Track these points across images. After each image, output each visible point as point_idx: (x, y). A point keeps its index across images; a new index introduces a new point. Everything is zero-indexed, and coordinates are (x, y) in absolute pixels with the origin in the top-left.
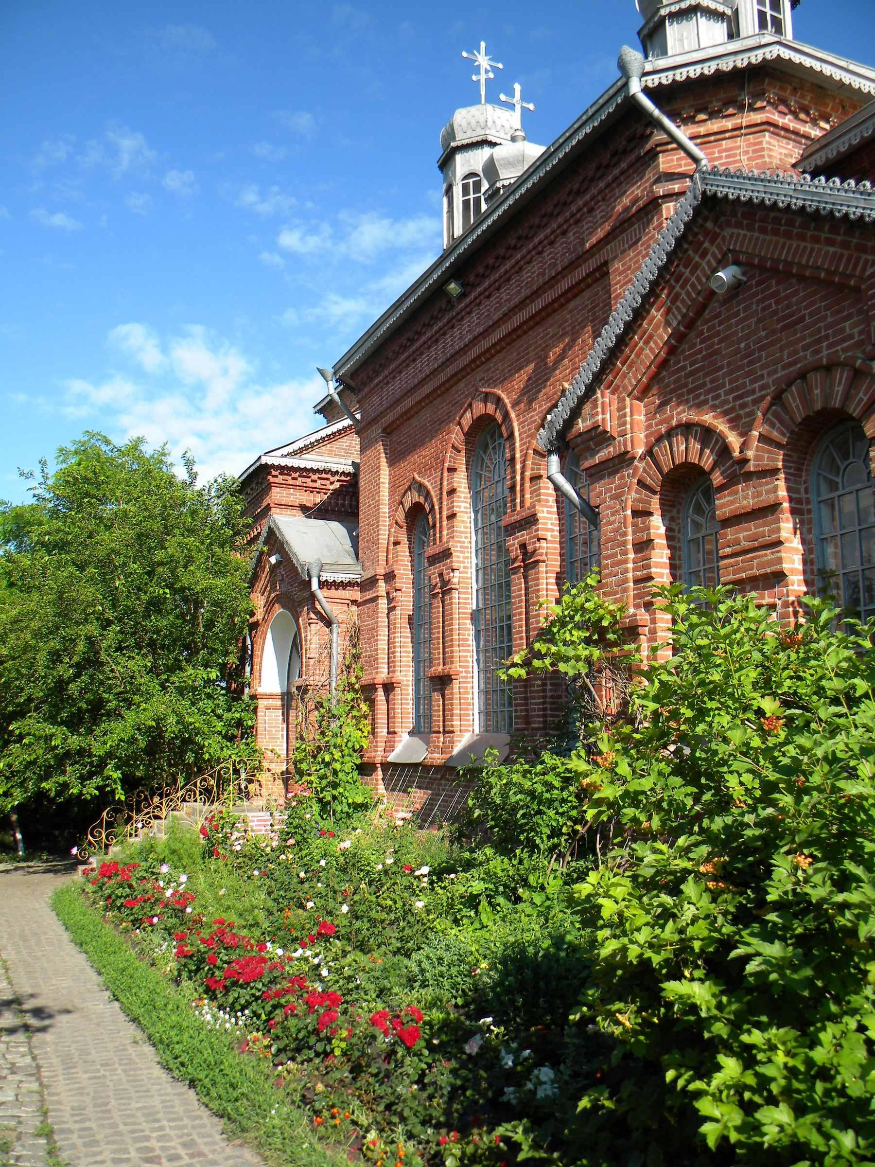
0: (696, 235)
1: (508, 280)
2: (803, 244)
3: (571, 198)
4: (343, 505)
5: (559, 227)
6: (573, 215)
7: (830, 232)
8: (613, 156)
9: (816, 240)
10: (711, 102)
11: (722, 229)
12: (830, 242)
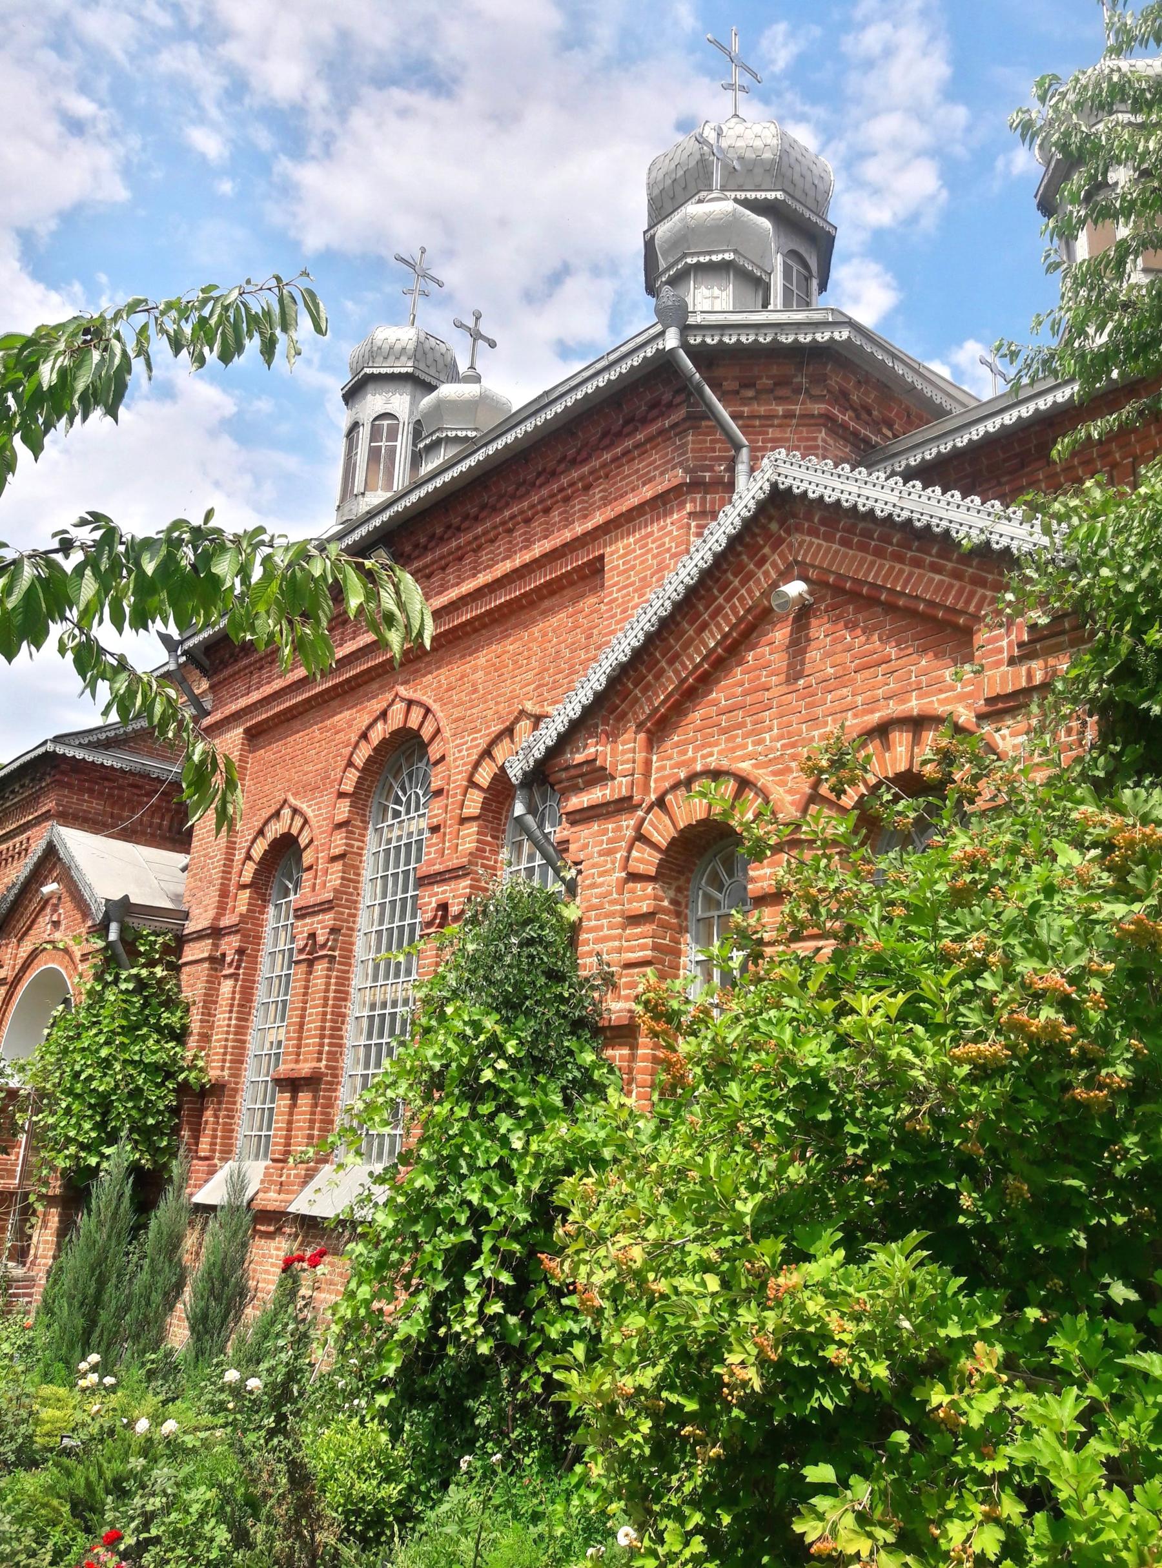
0: (754, 536)
1: (461, 559)
2: (898, 566)
3: (562, 466)
4: (160, 826)
5: (541, 501)
6: (561, 490)
7: (939, 556)
8: (627, 422)
9: (917, 563)
10: (760, 378)
11: (789, 534)
12: (936, 569)
